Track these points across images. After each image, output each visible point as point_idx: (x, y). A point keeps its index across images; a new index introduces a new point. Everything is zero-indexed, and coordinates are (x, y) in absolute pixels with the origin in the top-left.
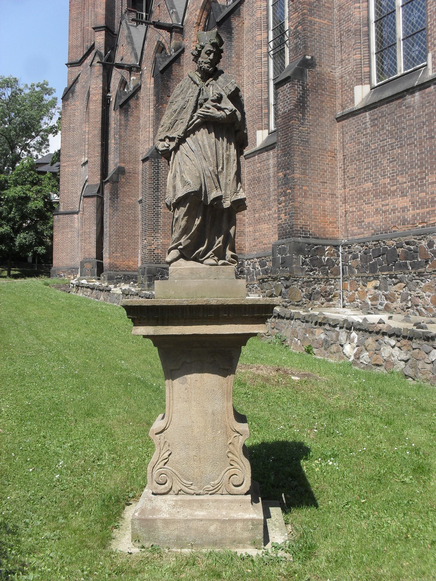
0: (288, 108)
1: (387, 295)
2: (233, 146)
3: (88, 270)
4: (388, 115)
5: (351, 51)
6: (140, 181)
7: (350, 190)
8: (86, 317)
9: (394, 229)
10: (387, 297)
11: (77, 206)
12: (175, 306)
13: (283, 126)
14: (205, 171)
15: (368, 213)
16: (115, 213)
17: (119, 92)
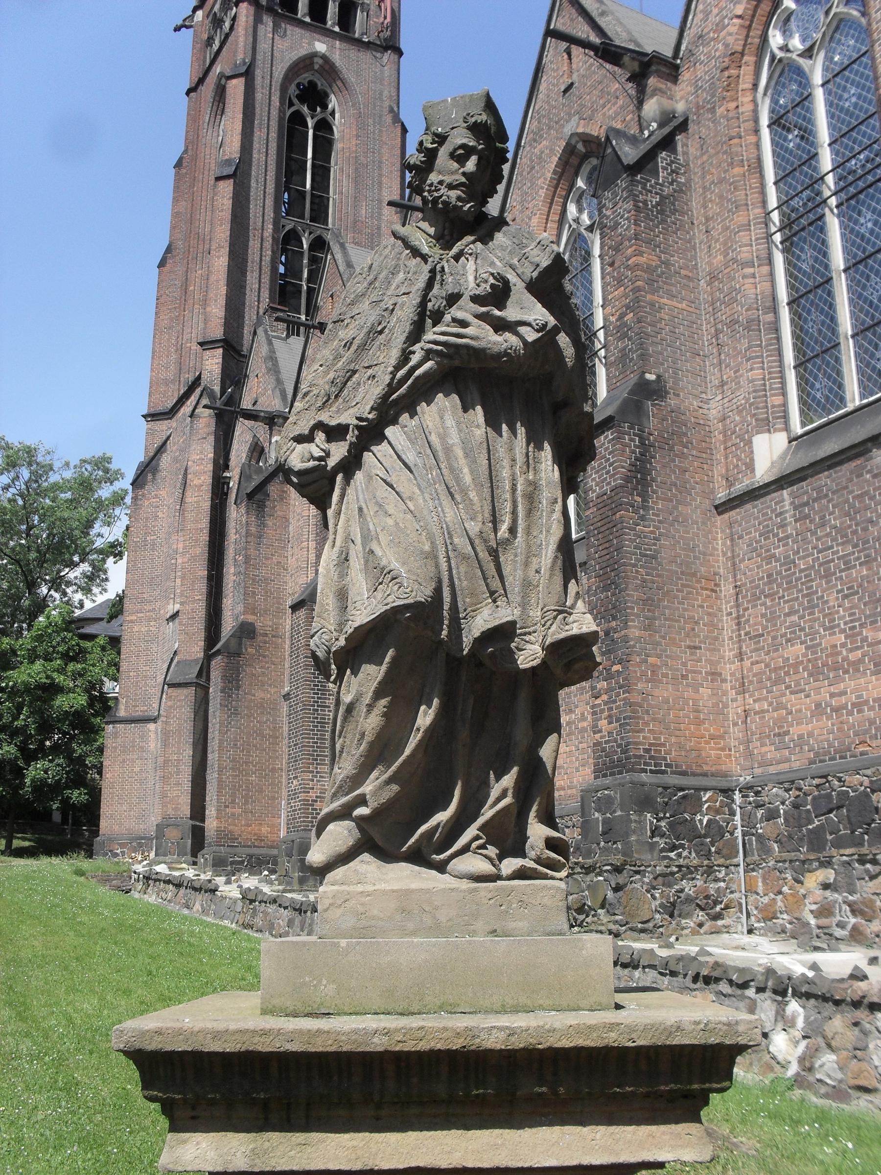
0: (609, 483)
1: (855, 902)
2: (547, 453)
3: (173, 843)
4: (833, 493)
5: (742, 363)
6: (287, 653)
7: (752, 664)
8: (151, 957)
9: (862, 748)
10: (855, 907)
11: (156, 706)
12: (338, 1056)
13: (599, 524)
14: (451, 537)
15: (799, 714)
16: (232, 720)
17: (246, 466)
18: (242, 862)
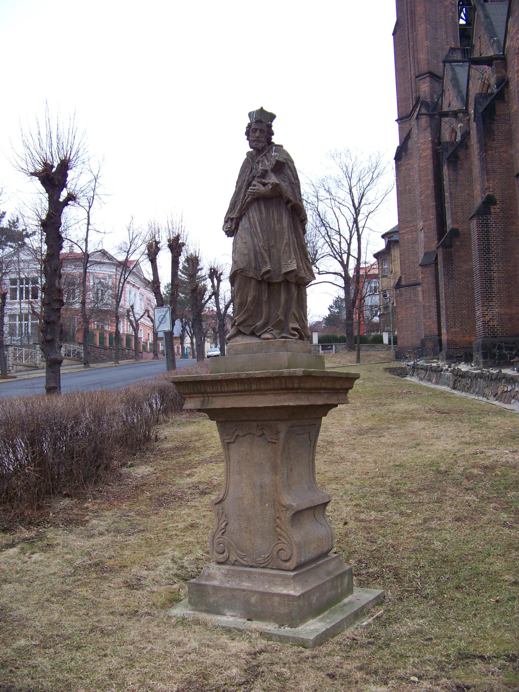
18: (462, 357)
